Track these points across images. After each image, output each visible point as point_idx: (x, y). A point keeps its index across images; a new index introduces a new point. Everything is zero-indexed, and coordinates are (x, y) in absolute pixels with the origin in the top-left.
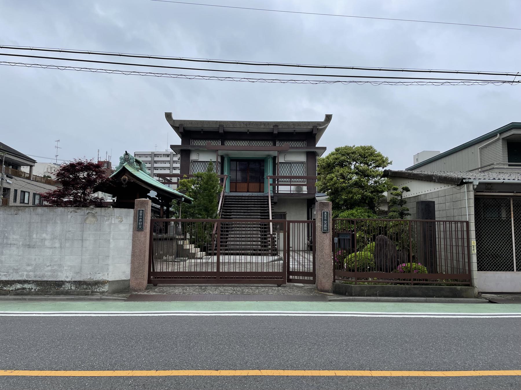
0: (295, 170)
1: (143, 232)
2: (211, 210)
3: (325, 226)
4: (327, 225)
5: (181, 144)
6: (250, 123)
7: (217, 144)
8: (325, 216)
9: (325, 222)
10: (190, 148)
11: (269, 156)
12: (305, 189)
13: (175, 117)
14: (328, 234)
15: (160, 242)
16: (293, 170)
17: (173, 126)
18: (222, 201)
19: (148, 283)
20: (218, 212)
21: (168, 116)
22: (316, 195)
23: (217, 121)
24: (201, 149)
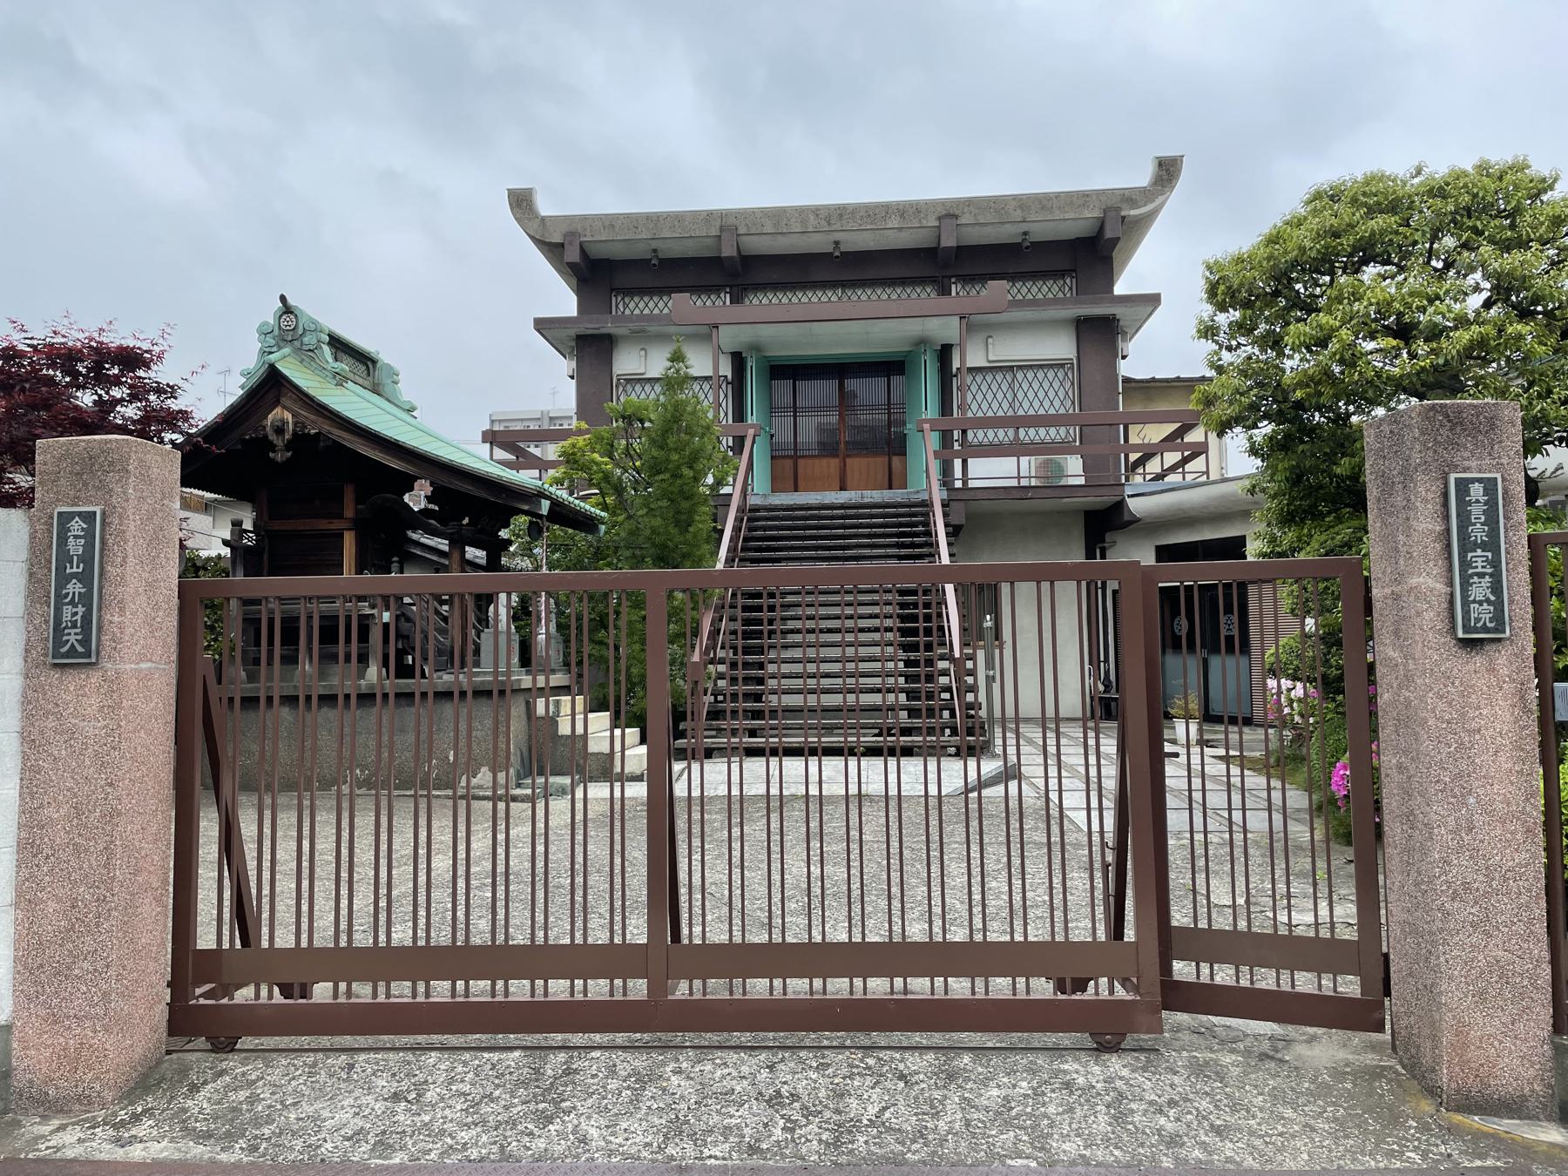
0: (1031, 395)
1: (95, 677)
3: (1480, 589)
4: (1496, 588)
7: (717, 305)
8: (1477, 511)
9: (1479, 559)
10: (609, 328)
11: (922, 342)
12: (1074, 469)
13: (546, 207)
14: (1502, 658)
15: (448, 709)
16: (1020, 395)
17: (541, 244)
18: (737, 529)
19: (170, 1034)
21: (521, 202)
22: (1128, 491)
24: (654, 329)
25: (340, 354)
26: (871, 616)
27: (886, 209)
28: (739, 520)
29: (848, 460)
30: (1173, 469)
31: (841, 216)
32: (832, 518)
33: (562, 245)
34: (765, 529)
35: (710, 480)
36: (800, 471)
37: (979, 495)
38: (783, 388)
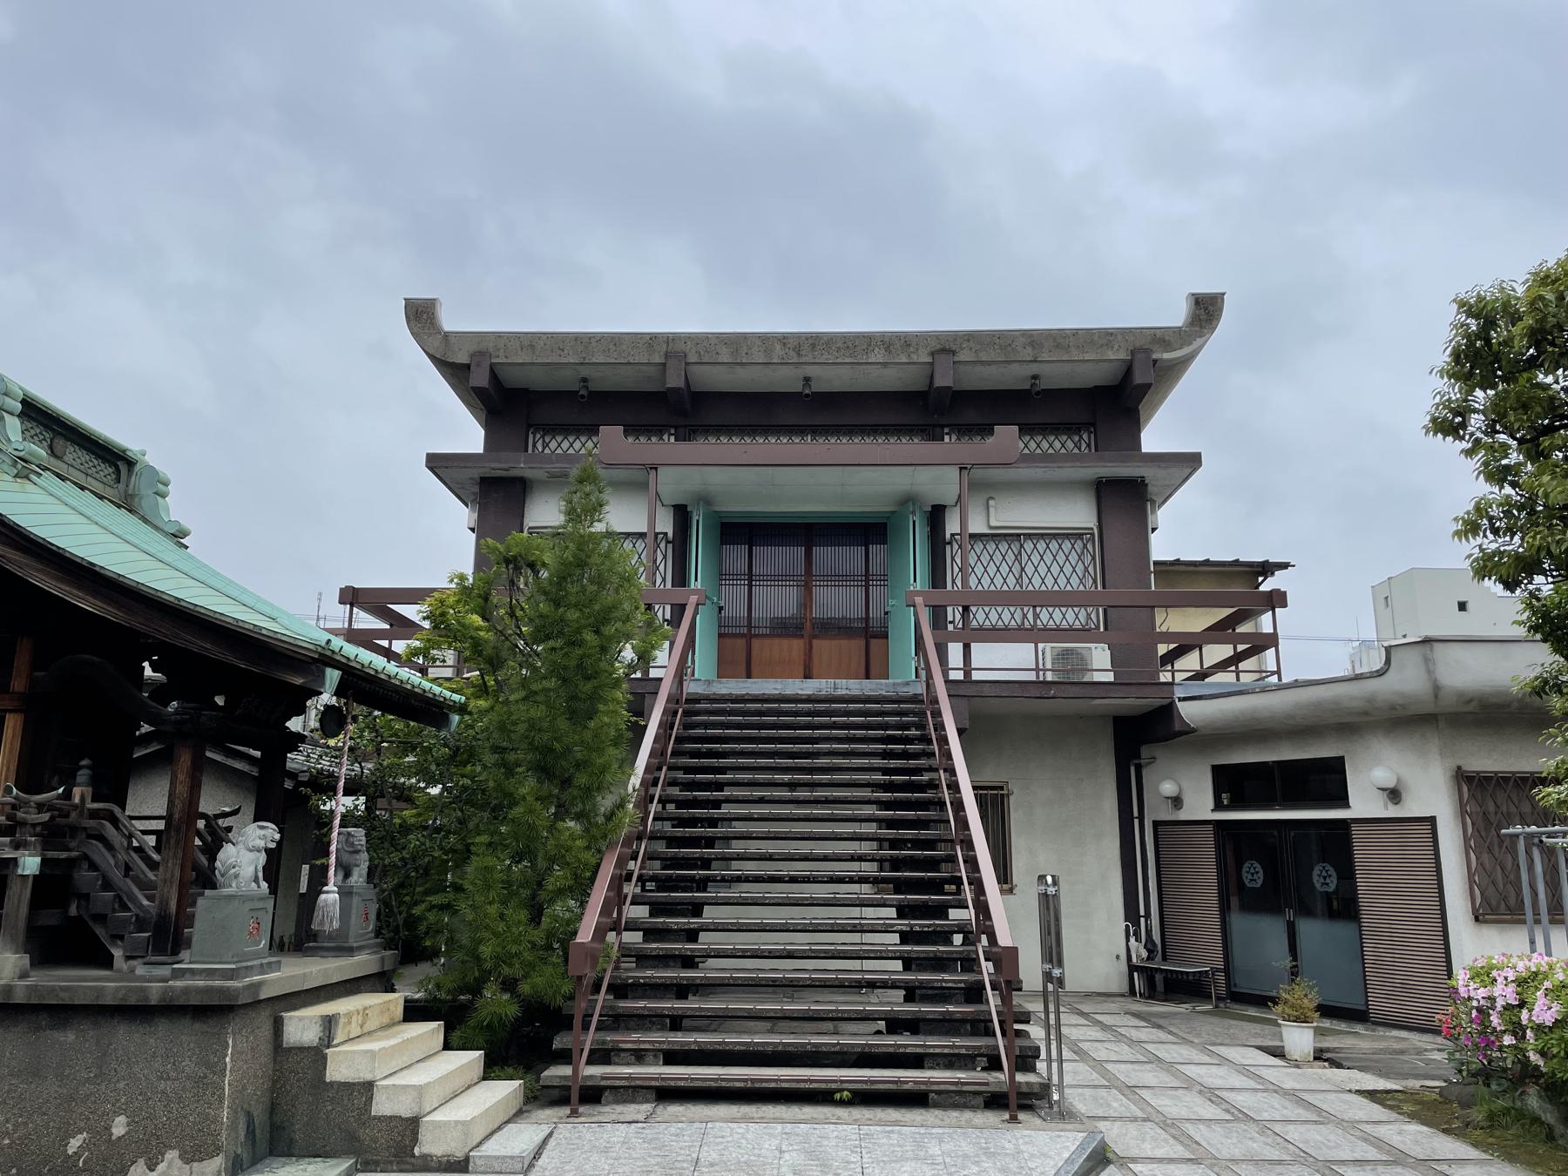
0: (1042, 569)
2: (578, 765)
5: (481, 451)
6: (815, 342)
10: (528, 474)
11: (908, 500)
12: (1100, 661)
13: (451, 321)
16: (1029, 569)
18: (666, 726)
20: (635, 781)
23: (654, 337)
25: (60, 443)
26: (852, 858)
27: (868, 341)
28: (670, 713)
29: (815, 642)
30: (1222, 666)
31: (813, 346)
32: (848, 714)
33: (468, 367)
34: (706, 726)
35: (628, 654)
36: (754, 653)
37: (987, 690)
38: (736, 555)
